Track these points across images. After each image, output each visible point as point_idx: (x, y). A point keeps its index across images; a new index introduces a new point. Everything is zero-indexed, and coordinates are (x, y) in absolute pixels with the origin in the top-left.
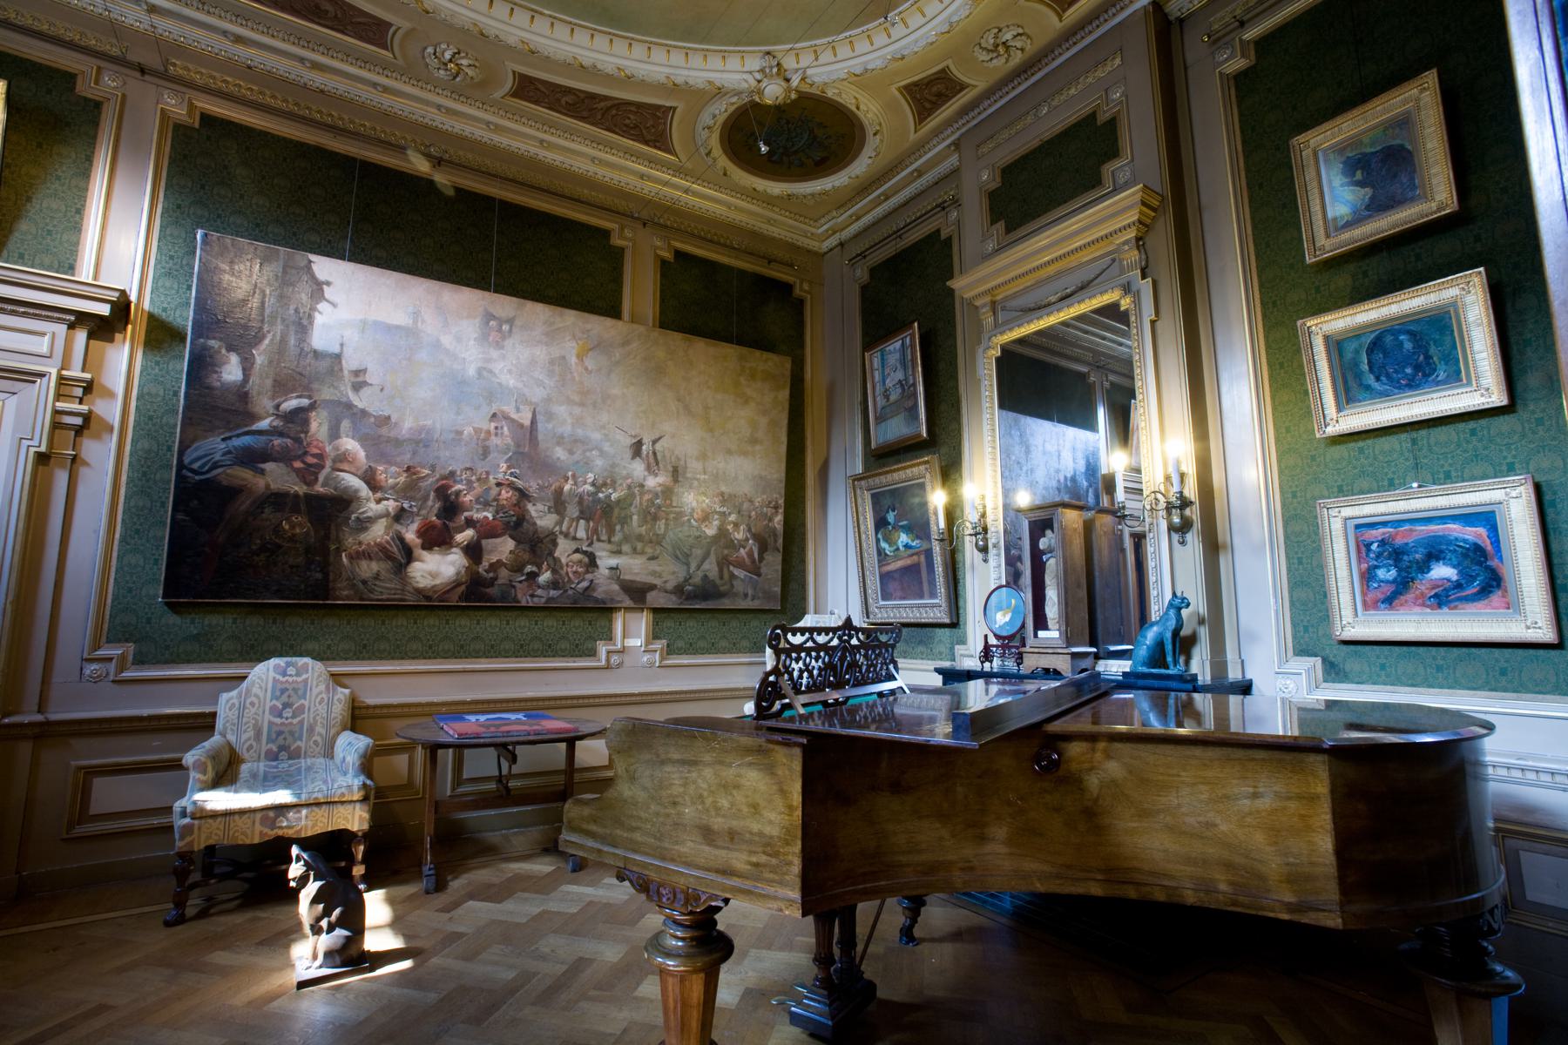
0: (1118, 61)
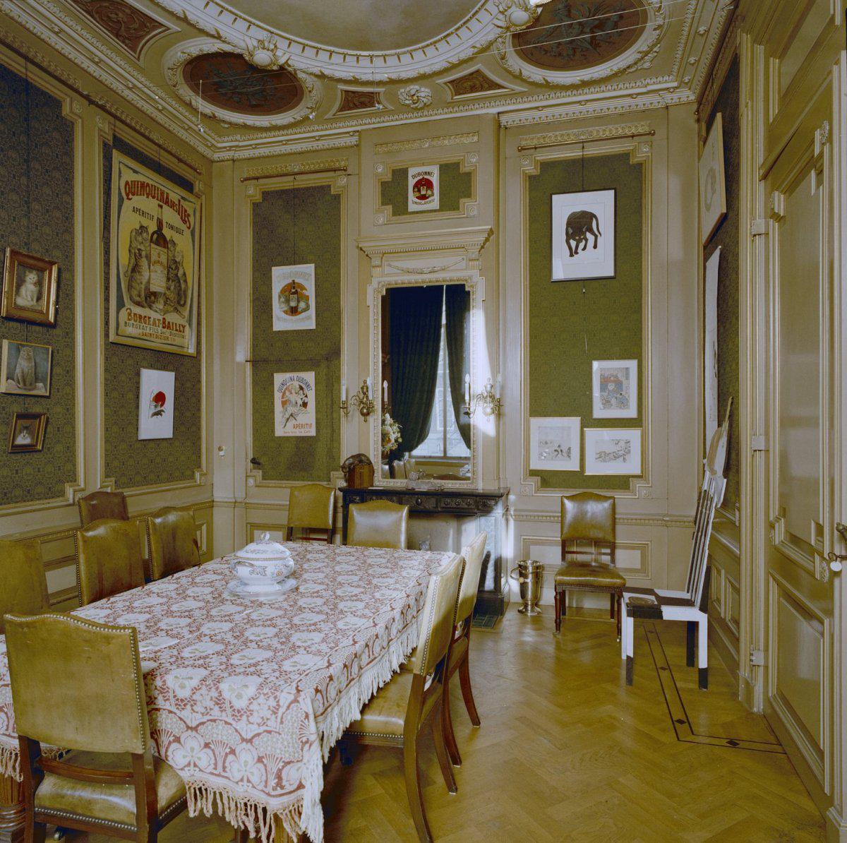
0: (476, 139)
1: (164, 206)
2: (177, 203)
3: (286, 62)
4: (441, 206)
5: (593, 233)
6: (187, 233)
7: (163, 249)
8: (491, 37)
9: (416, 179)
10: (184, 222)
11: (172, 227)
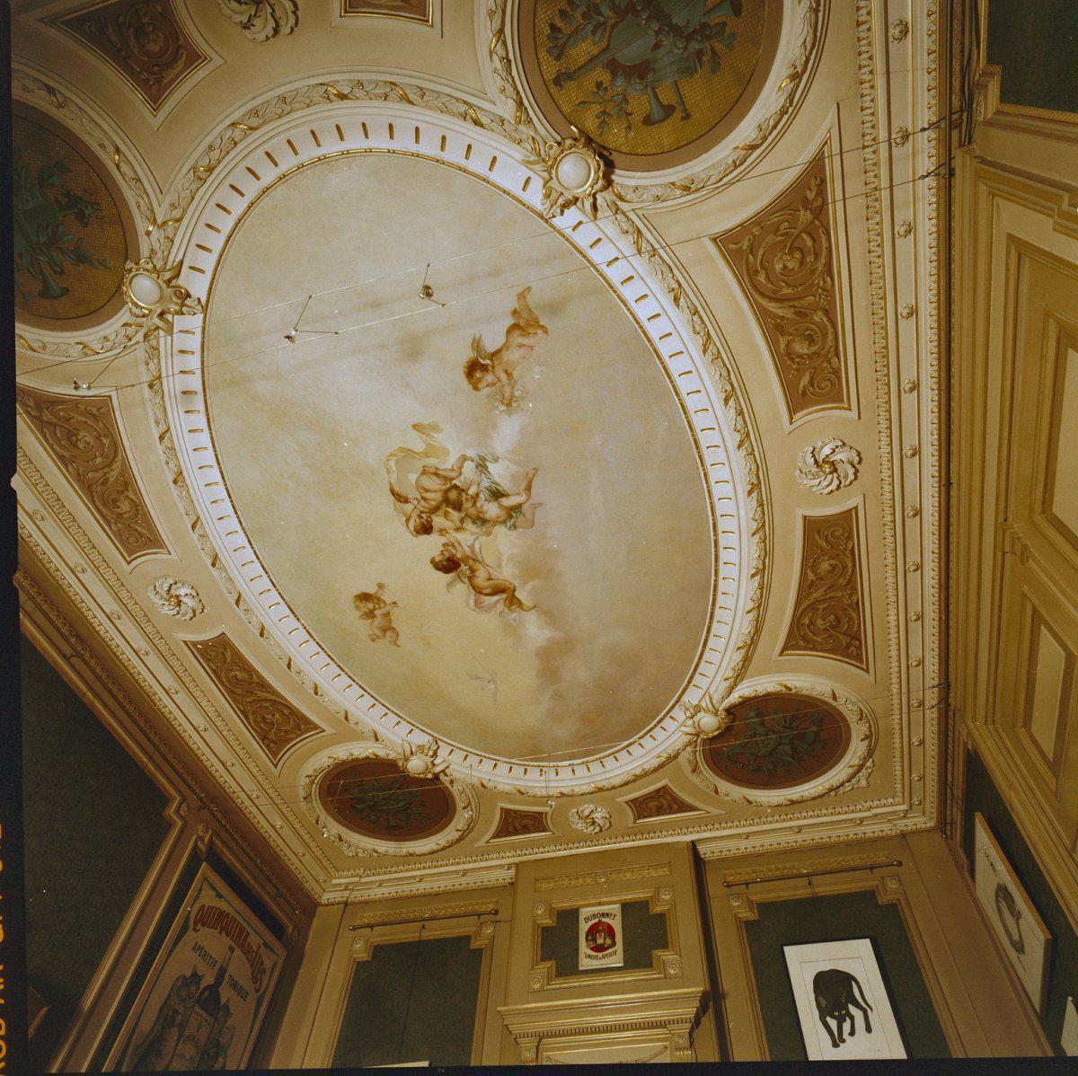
1: (237, 949)
2: (255, 949)
3: (443, 771)
4: (626, 960)
5: (858, 1005)
6: (252, 998)
7: (209, 1019)
8: (679, 745)
9: (590, 924)
10: (255, 980)
11: (234, 985)
